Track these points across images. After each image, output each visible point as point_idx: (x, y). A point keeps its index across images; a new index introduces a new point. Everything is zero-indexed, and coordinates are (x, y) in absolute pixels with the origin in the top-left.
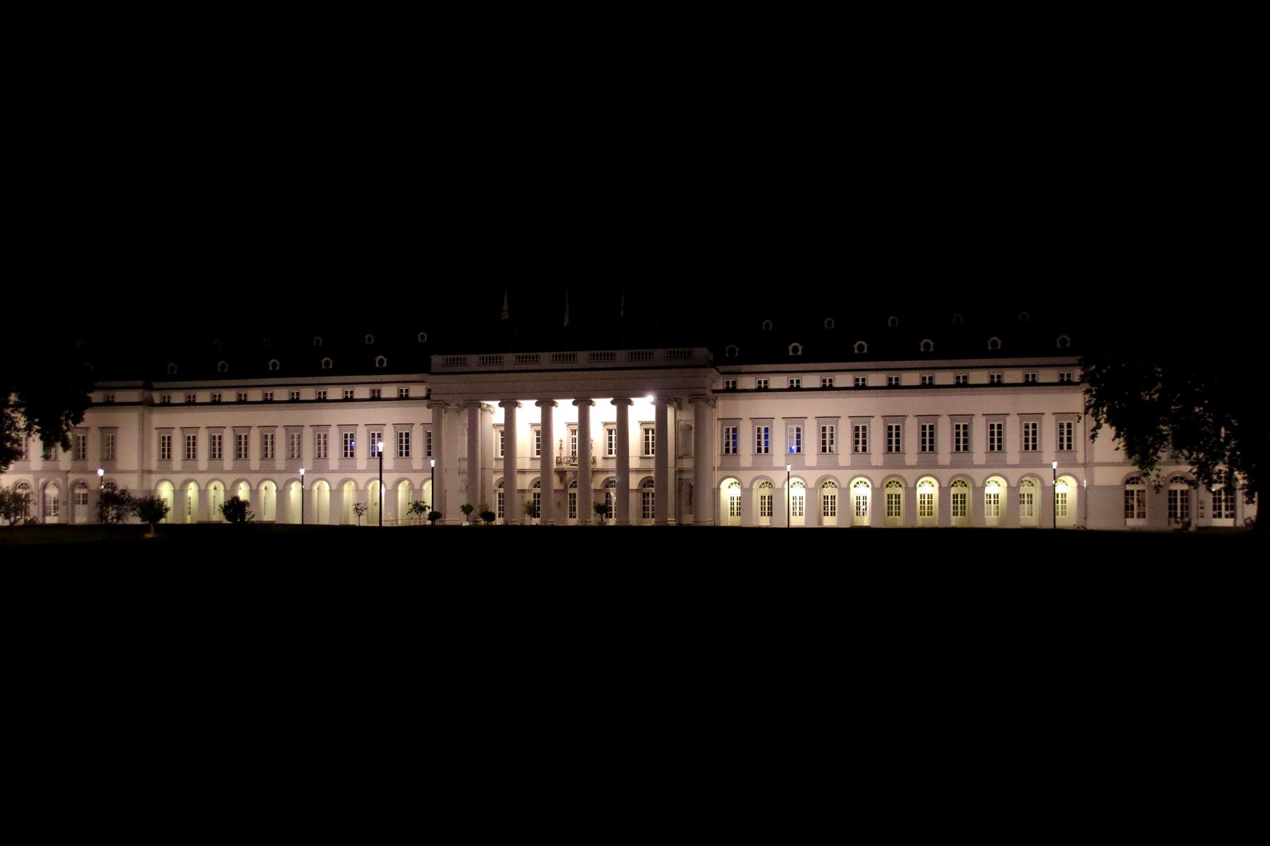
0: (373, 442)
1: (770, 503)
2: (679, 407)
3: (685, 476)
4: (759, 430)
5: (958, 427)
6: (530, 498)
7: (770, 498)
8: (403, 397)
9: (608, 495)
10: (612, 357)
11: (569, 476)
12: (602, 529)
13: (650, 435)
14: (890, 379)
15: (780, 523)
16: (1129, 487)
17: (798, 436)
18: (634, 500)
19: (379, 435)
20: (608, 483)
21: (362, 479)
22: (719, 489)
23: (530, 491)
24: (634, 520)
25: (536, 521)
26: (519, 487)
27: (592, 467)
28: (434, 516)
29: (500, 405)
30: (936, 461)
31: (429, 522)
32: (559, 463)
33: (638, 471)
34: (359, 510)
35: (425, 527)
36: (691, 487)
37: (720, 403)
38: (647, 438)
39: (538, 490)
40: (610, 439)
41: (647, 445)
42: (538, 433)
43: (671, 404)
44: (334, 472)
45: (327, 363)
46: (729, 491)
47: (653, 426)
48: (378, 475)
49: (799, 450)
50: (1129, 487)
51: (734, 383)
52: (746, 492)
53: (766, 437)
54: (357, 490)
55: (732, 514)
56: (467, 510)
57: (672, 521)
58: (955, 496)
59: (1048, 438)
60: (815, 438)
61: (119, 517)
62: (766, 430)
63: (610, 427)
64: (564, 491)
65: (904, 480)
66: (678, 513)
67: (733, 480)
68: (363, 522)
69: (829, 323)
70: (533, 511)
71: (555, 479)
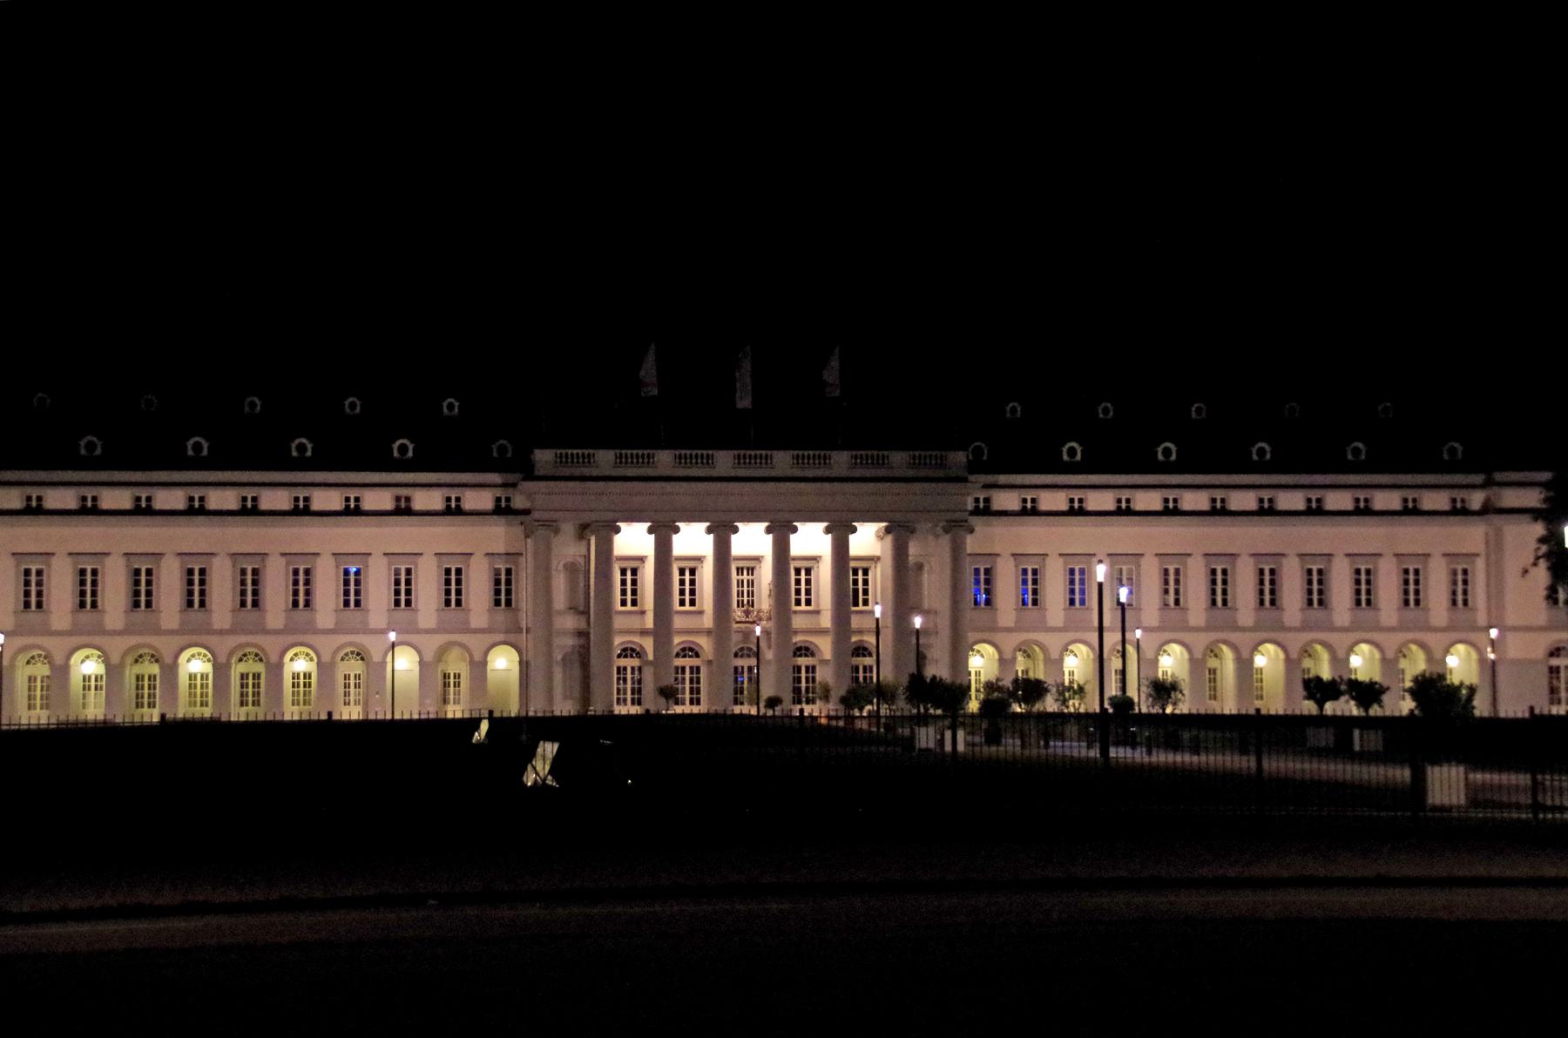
5: (1025, 571)
10: (649, 461)
14: (138, 499)
16: (1555, 662)
30: (209, 624)
44: (1009, 630)
45: (403, 449)
50: (1555, 662)
58: (243, 676)
59: (378, 591)
60: (228, 584)
62: (307, 572)
65: (263, 650)
69: (450, 406)
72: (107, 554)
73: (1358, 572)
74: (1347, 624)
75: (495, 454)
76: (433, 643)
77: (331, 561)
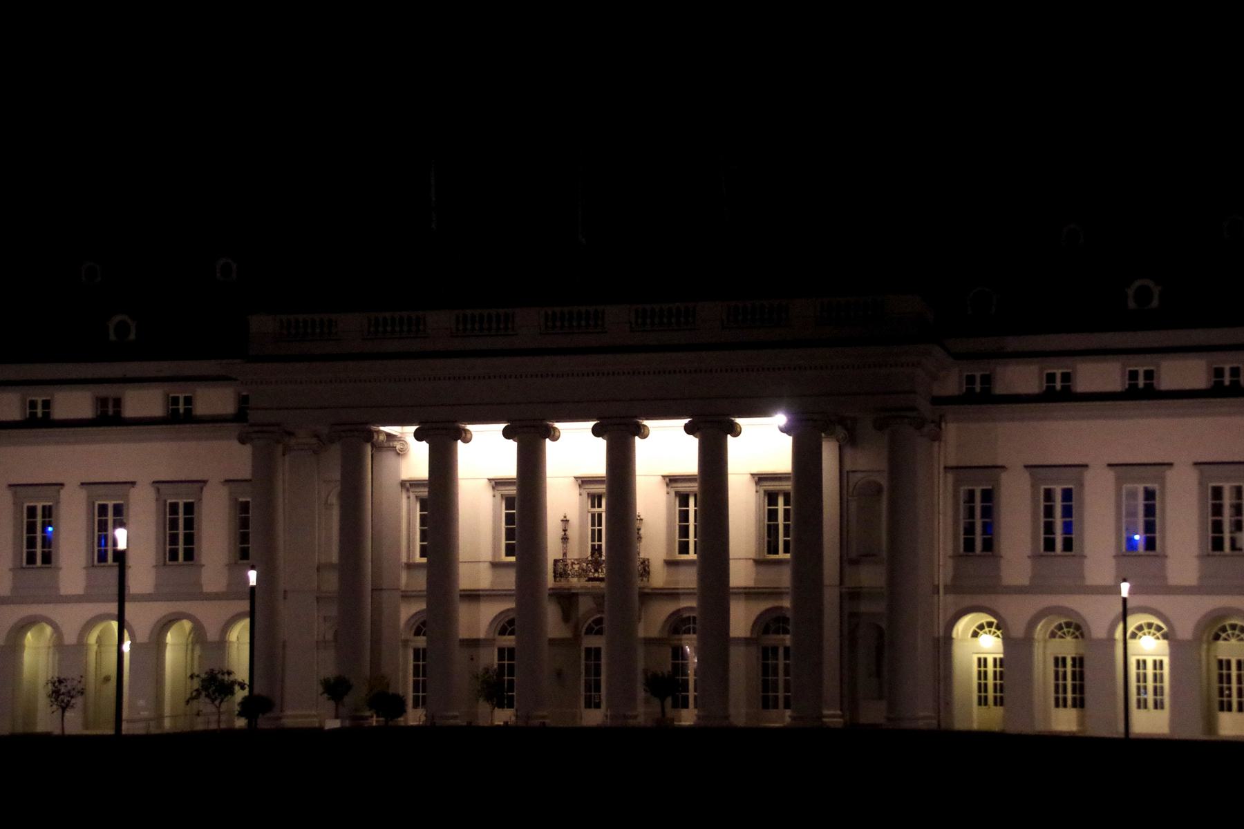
0: (103, 526)
1: (1079, 676)
2: (850, 441)
3: (865, 607)
4: (1049, 495)
6: (490, 658)
7: (1079, 662)
8: (179, 418)
9: (678, 653)
11: (585, 605)
12: (664, 731)
13: (781, 507)
15: (1106, 727)
16: (772, 639)
17: (1150, 511)
18: (741, 664)
19: (118, 510)
20: (678, 624)
21: (71, 617)
22: (949, 639)
23: (488, 642)
24: (740, 713)
25: (503, 717)
26: (463, 634)
27: (639, 583)
28: (253, 706)
29: (419, 436)
31: (241, 723)
32: (560, 573)
33: (749, 594)
34: (62, 693)
35: (231, 732)
36: (880, 633)
37: (951, 430)
38: (772, 515)
39: (509, 641)
40: (684, 516)
41: (772, 530)
42: (510, 503)
43: (830, 434)
46: (977, 644)
47: (788, 486)
48: (113, 608)
49: (1150, 544)
51: (1066, 377)
52: (1017, 648)
53: (1067, 512)
54: (59, 645)
55: (983, 701)
56: (336, 689)
57: (832, 716)
61: (242, 686)
62: (1067, 495)
63: (772, 486)
64: (576, 640)
66: (850, 701)
67: (985, 618)
68: (74, 724)
70: (496, 689)
71: (552, 614)
72: (1171, 465)
73: (103, 509)
74: (1026, 582)
75: (112, 337)
76: (1190, 612)
77: (1025, 480)
